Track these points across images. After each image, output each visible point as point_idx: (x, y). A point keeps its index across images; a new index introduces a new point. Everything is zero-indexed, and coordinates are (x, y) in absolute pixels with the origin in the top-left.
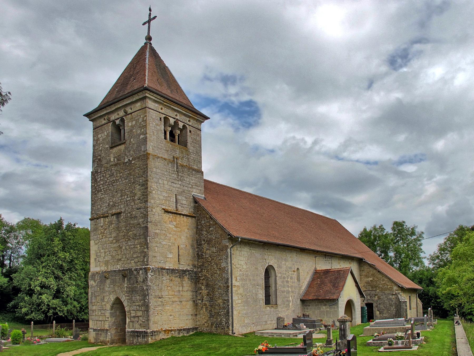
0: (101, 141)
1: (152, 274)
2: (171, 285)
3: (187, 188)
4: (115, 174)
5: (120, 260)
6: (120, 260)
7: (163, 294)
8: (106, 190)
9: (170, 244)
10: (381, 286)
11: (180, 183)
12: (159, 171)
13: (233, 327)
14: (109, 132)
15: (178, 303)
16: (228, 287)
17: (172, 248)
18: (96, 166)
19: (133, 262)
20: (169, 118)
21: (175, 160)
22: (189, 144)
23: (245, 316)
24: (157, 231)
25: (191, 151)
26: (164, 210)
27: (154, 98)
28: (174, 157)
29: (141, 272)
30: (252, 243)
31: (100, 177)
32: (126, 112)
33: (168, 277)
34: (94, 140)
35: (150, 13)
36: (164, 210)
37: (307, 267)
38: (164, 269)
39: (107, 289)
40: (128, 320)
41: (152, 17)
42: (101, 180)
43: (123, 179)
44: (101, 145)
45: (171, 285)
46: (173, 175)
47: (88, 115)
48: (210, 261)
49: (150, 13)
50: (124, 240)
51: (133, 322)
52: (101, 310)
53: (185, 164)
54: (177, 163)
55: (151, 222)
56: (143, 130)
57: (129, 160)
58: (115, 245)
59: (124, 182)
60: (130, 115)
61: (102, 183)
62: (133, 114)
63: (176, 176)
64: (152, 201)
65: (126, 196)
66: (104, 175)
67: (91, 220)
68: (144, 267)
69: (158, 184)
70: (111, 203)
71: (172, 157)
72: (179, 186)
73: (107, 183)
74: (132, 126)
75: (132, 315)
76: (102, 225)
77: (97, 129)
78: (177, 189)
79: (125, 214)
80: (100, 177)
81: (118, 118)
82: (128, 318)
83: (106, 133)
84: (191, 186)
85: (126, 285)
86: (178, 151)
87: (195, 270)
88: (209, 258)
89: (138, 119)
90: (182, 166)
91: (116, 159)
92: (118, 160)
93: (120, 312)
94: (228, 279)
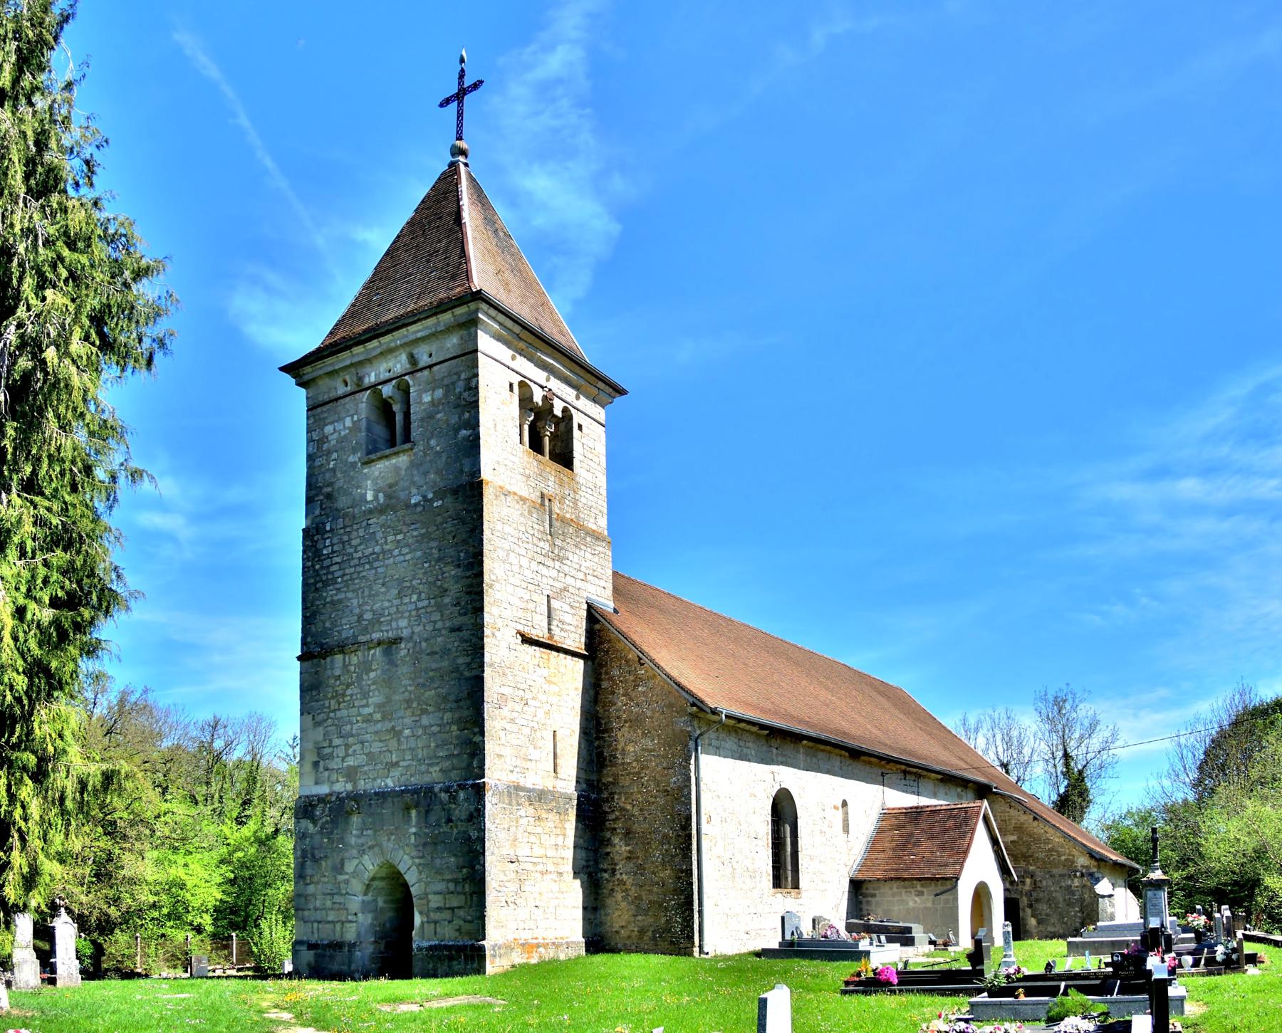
0: (333, 442)
2: (539, 830)
4: (380, 535)
5: (396, 764)
6: (396, 764)
8: (352, 579)
9: (535, 724)
10: (1042, 855)
11: (557, 564)
13: (701, 939)
14: (359, 420)
15: (554, 876)
16: (690, 836)
17: (538, 734)
18: (317, 512)
19: (437, 769)
21: (547, 502)
22: (576, 462)
24: (506, 690)
26: (522, 635)
28: (542, 496)
29: (462, 795)
30: (743, 730)
31: (332, 545)
32: (413, 359)
33: (531, 811)
34: (310, 440)
35: (463, 70)
36: (522, 635)
37: (873, 800)
38: (524, 789)
39: (353, 841)
40: (418, 919)
41: (468, 82)
42: (333, 552)
43: (405, 550)
44: (335, 455)
45: (539, 830)
46: (542, 544)
47: (286, 369)
48: (639, 773)
49: (463, 70)
50: (409, 712)
51: (436, 923)
52: (332, 895)
53: (568, 516)
54: (550, 511)
56: (467, 415)
57: (424, 497)
58: (379, 726)
59: (408, 557)
60: (426, 372)
61: (338, 559)
62: (435, 368)
63: (547, 546)
65: (415, 597)
66: (346, 538)
67: (299, 658)
68: (470, 782)
70: (368, 616)
71: (539, 494)
72: (554, 573)
73: (356, 562)
74: (432, 402)
75: (433, 905)
76: (337, 672)
77: (319, 410)
78: (551, 581)
79: (411, 645)
80: (332, 545)
81: (390, 380)
82: (421, 913)
83: (348, 422)
84: (581, 576)
85: (413, 830)
86: (552, 478)
87: (593, 796)
88: (635, 764)
89: (453, 383)
90: (563, 520)
91: (381, 495)
92: (388, 496)
93: (385, 902)
94: (689, 818)
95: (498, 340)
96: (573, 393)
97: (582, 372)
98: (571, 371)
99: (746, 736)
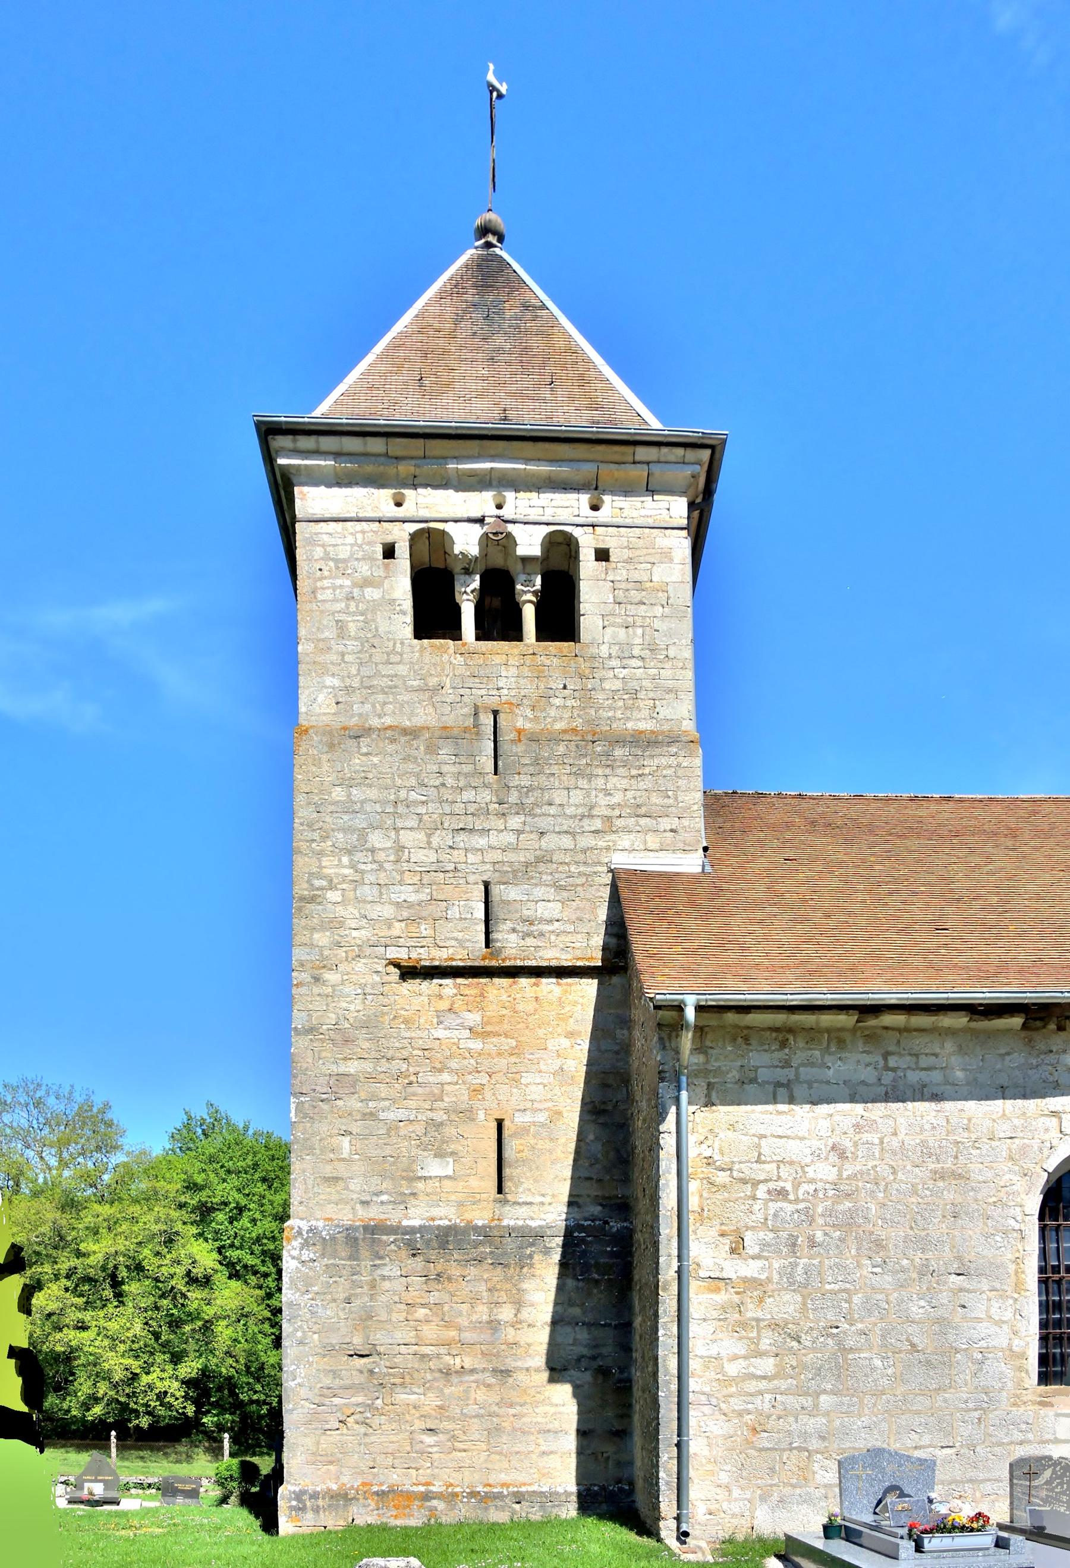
1: (306, 1255)
3: (567, 842)
7: (379, 1337)
11: (515, 822)
12: (372, 793)
20: (449, 527)
23: (815, 1444)
25: (604, 650)
27: (544, 469)
36: (397, 965)
55: (311, 1030)
64: (322, 939)
69: (359, 856)
72: (511, 838)
95: (349, 484)
96: (385, 496)
97: (581, 450)
98: (551, 461)
99: (918, 1042)
